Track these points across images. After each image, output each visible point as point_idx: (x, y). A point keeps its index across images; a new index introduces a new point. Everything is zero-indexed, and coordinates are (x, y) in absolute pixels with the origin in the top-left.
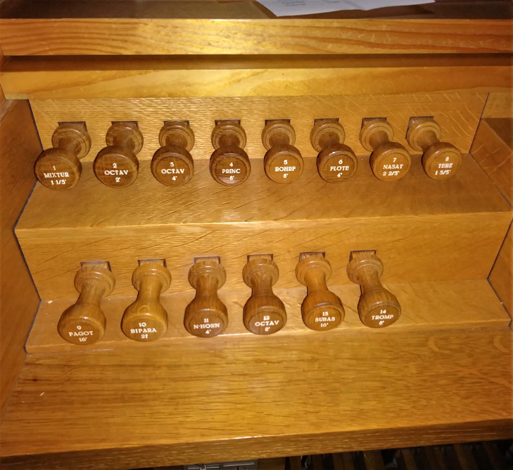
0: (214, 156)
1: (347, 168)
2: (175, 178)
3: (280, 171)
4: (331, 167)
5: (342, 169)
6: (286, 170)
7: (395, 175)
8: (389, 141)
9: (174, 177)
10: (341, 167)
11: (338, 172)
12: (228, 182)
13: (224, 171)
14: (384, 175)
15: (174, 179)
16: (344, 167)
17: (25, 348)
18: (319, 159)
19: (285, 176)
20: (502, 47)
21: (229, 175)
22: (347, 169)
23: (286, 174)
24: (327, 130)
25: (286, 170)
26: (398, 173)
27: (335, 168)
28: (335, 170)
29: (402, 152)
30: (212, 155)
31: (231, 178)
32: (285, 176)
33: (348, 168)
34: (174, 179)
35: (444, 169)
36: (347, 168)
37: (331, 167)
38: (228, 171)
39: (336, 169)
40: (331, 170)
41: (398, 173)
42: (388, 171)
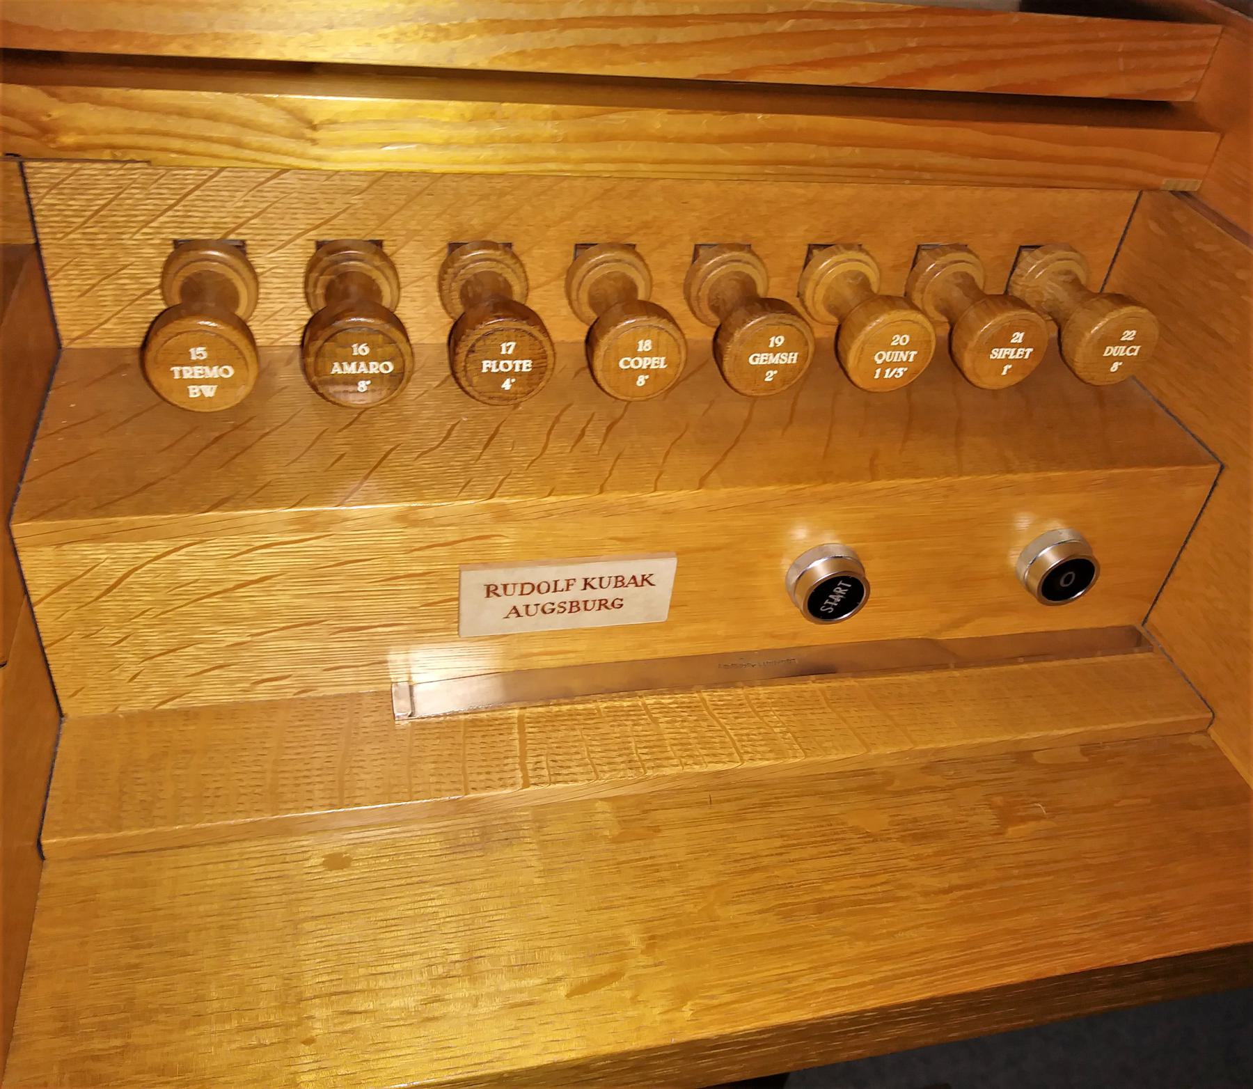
0: (313, 328)
1: (527, 365)
2: (511, 383)
3: (381, 373)
4: (485, 362)
5: (514, 368)
6: (792, 360)
7: (896, 376)
8: (758, 295)
9: (508, 381)
10: (509, 362)
11: (502, 376)
12: (353, 400)
13: (336, 369)
14: (767, 379)
15: (507, 385)
16: (518, 363)
17: (39, 845)
18: (591, 341)
19: (641, 381)
20: (25, 96)
21: (353, 380)
22: (528, 368)
23: (363, 382)
24: (483, 267)
25: (792, 360)
26: (646, 380)
27: (494, 366)
28: (494, 370)
29: (798, 325)
30: (307, 327)
31: (363, 386)
32: (641, 381)
33: (529, 365)
34: (507, 385)
35: (892, 365)
36: (527, 365)
37: (485, 362)
38: (374, 367)
39: (497, 367)
40: (485, 370)
41: (905, 373)
42: (886, 365)
